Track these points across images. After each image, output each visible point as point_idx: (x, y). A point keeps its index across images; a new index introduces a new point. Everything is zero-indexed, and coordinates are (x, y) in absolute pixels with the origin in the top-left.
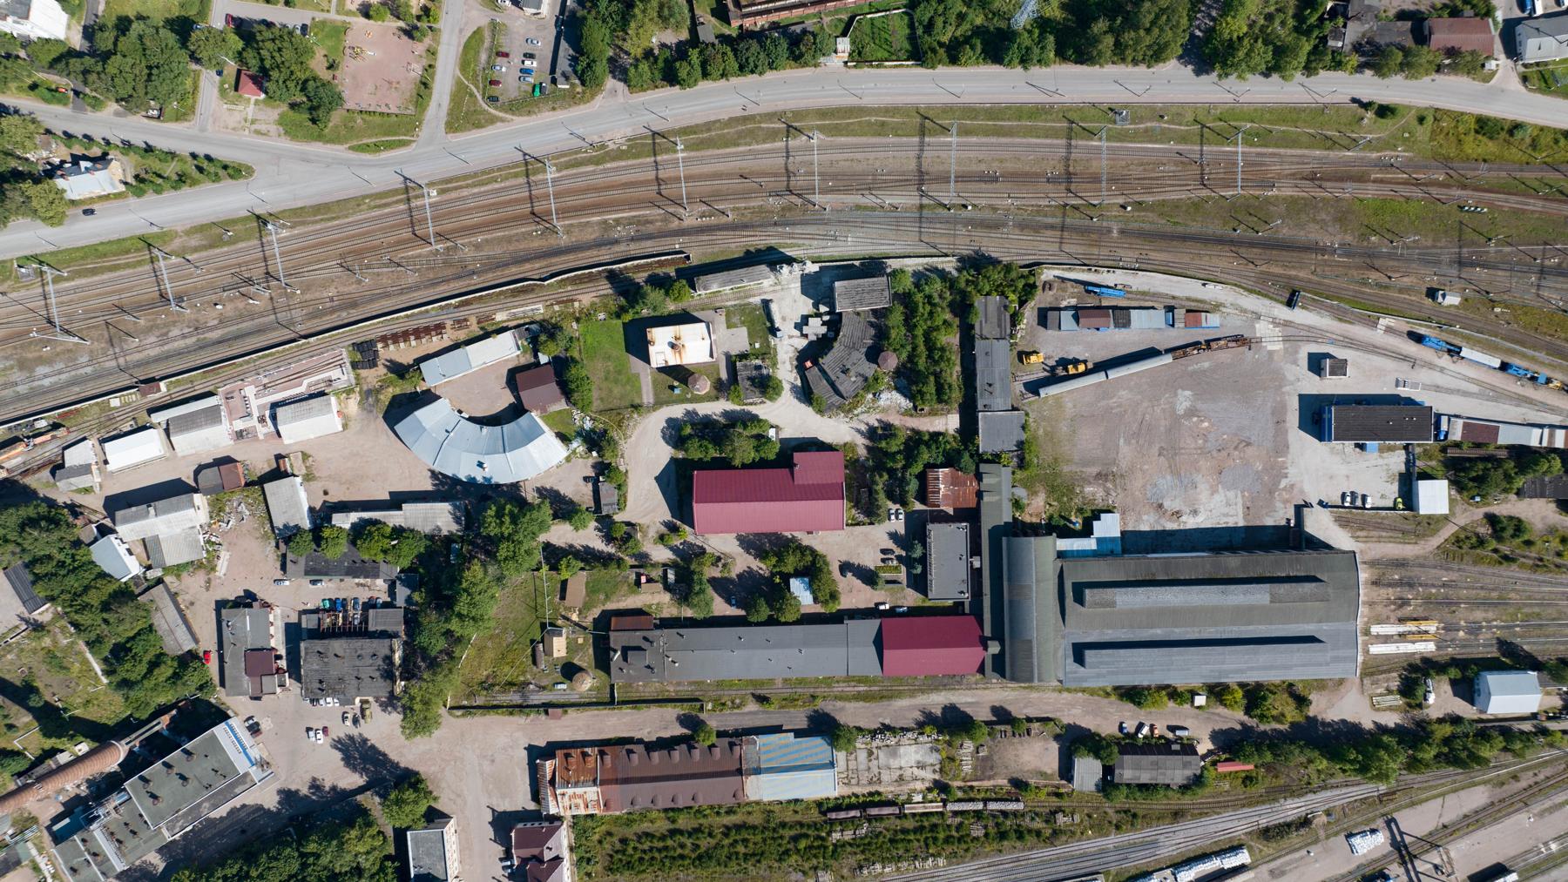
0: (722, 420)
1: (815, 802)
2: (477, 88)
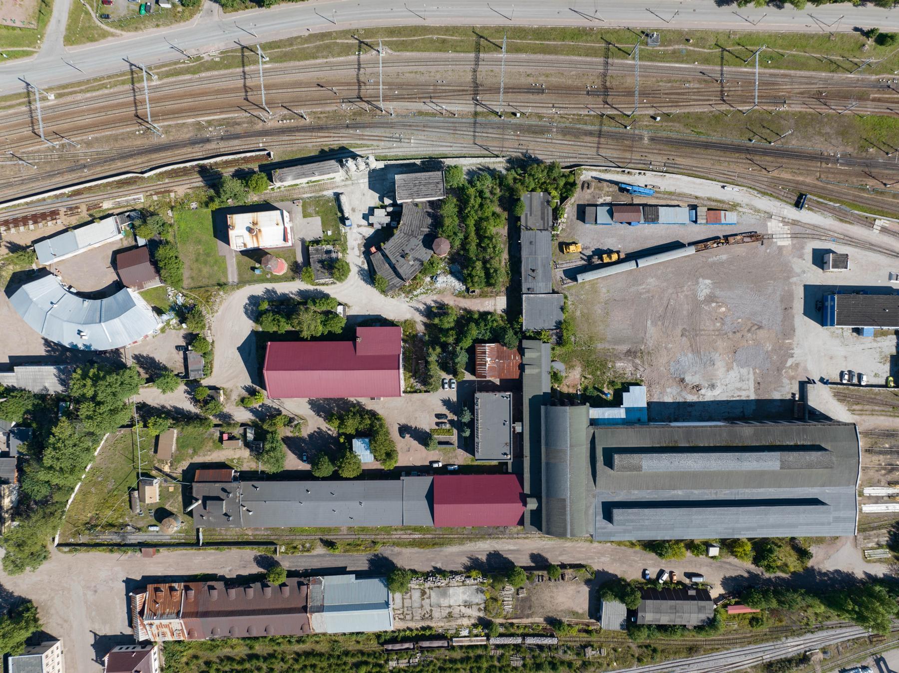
0: (298, 298)
1: (374, 634)
2: (92, 6)
